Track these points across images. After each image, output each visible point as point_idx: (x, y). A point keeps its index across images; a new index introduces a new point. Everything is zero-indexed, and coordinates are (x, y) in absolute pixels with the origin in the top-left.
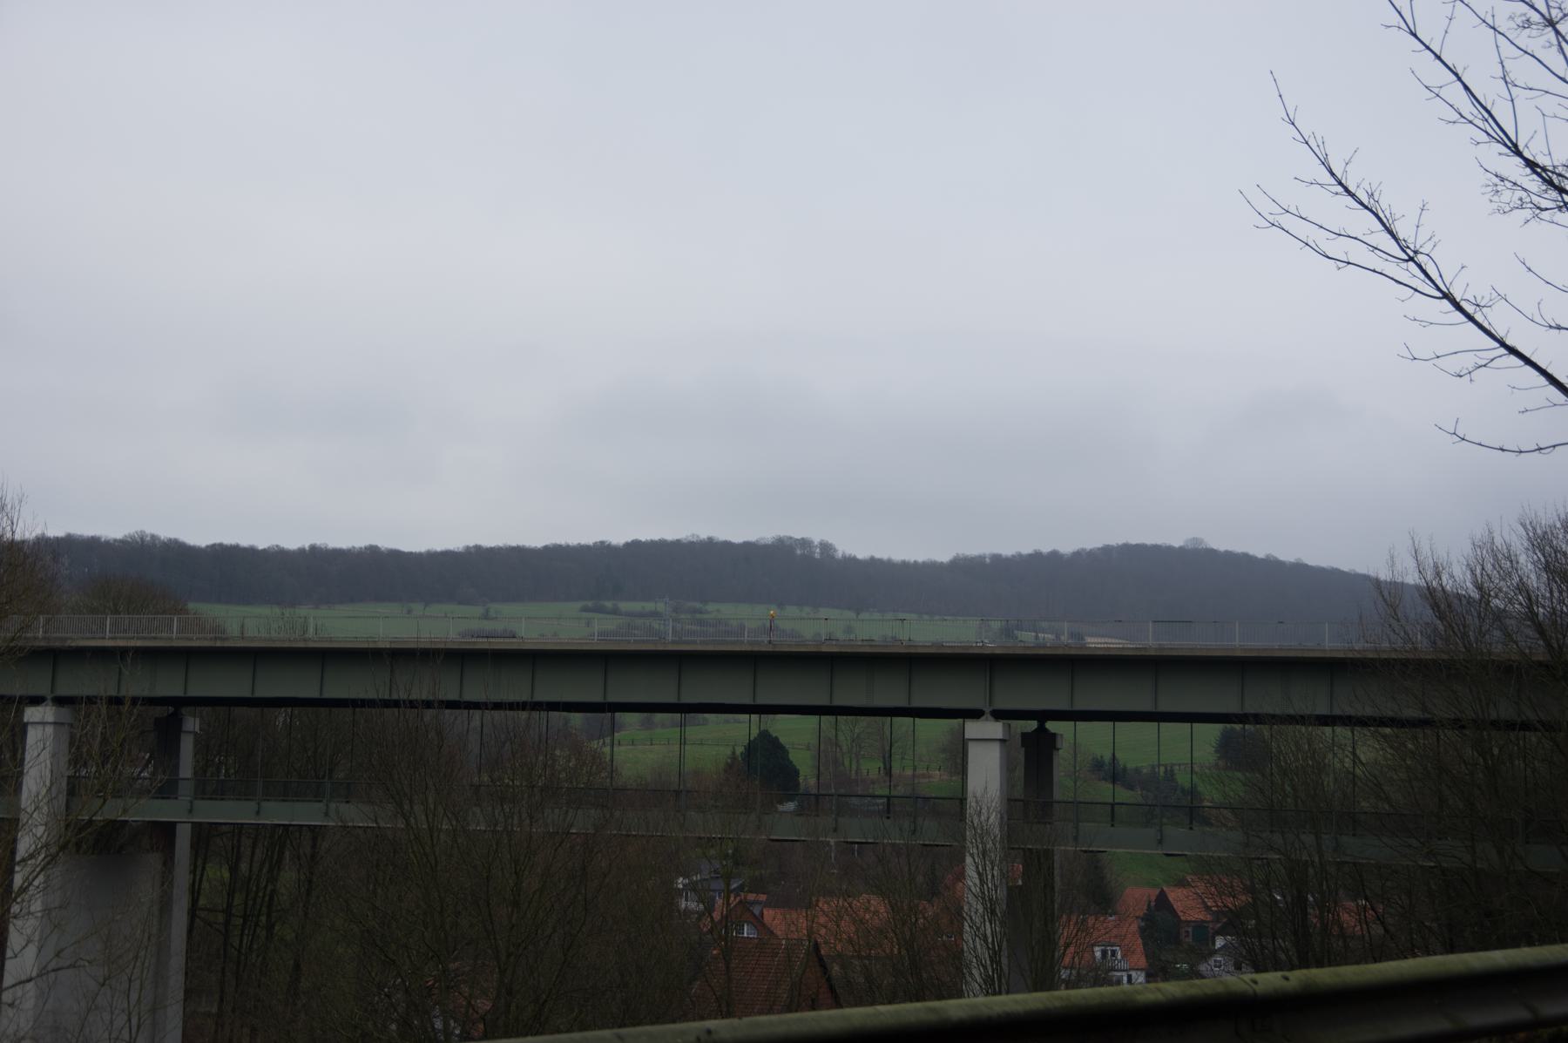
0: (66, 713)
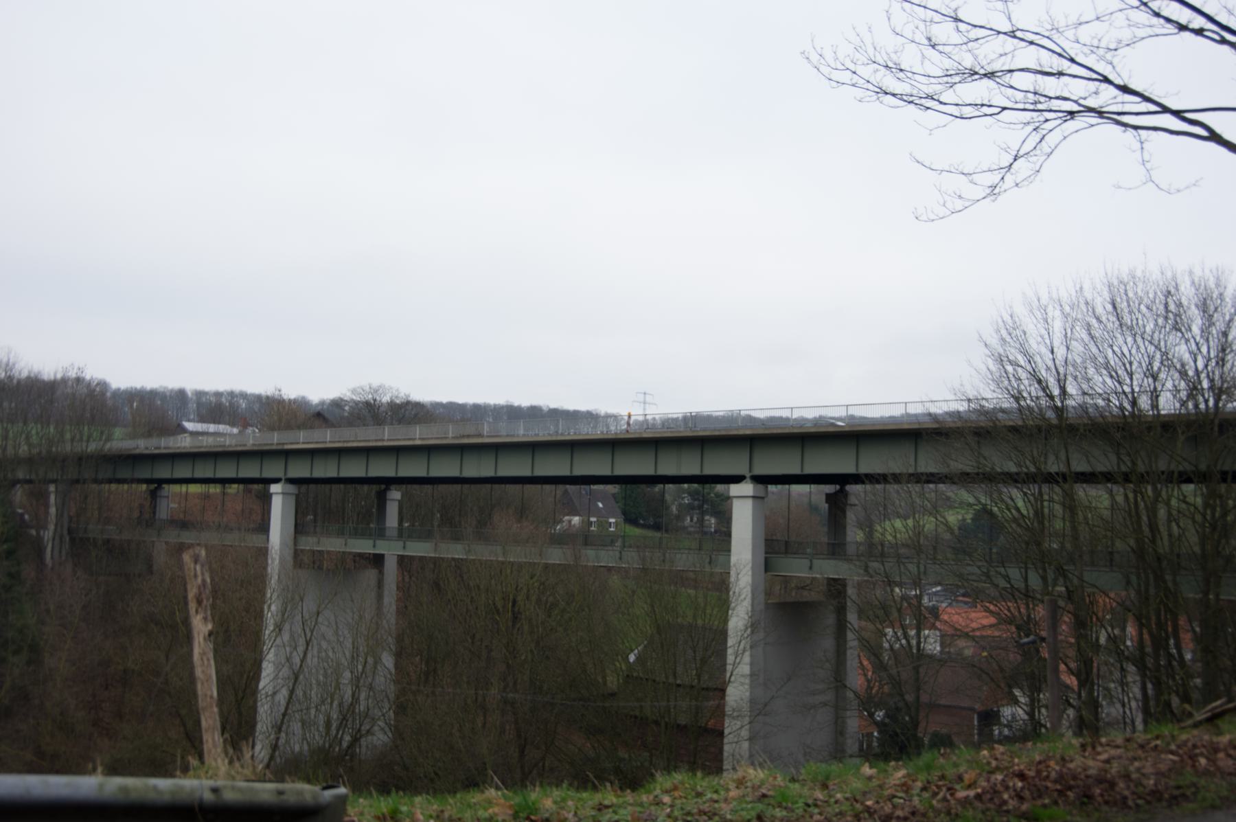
0: (292, 488)
